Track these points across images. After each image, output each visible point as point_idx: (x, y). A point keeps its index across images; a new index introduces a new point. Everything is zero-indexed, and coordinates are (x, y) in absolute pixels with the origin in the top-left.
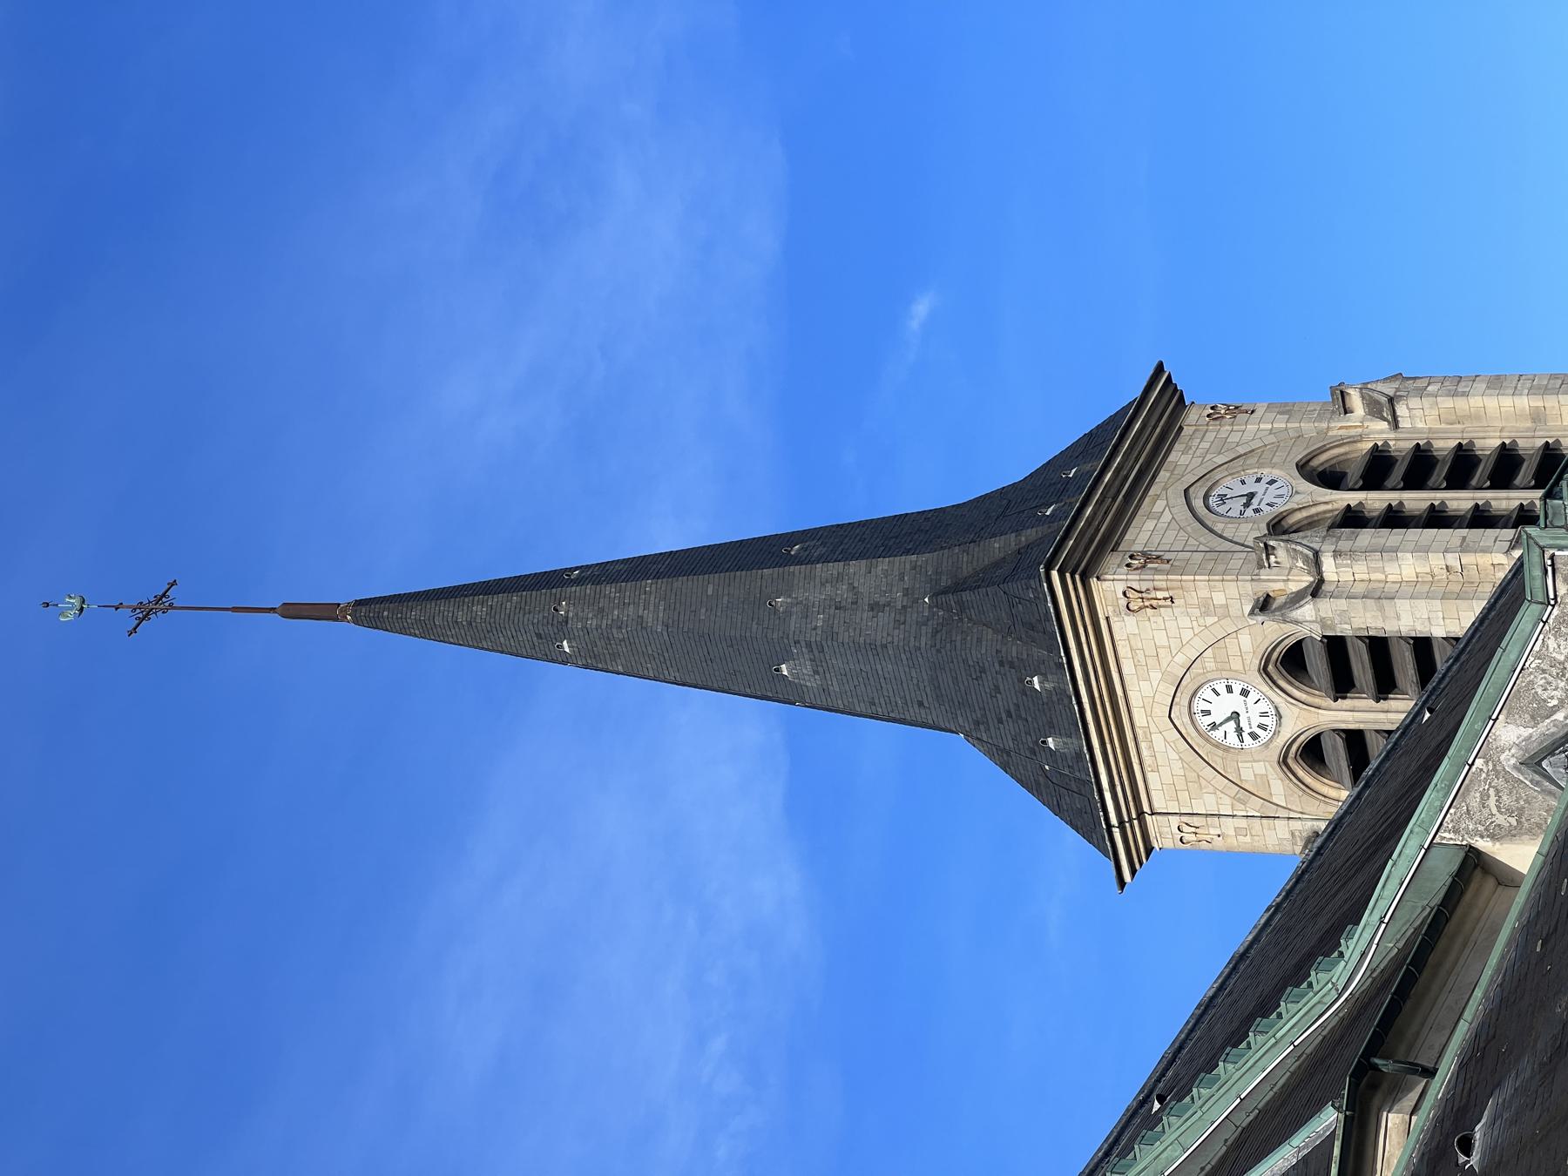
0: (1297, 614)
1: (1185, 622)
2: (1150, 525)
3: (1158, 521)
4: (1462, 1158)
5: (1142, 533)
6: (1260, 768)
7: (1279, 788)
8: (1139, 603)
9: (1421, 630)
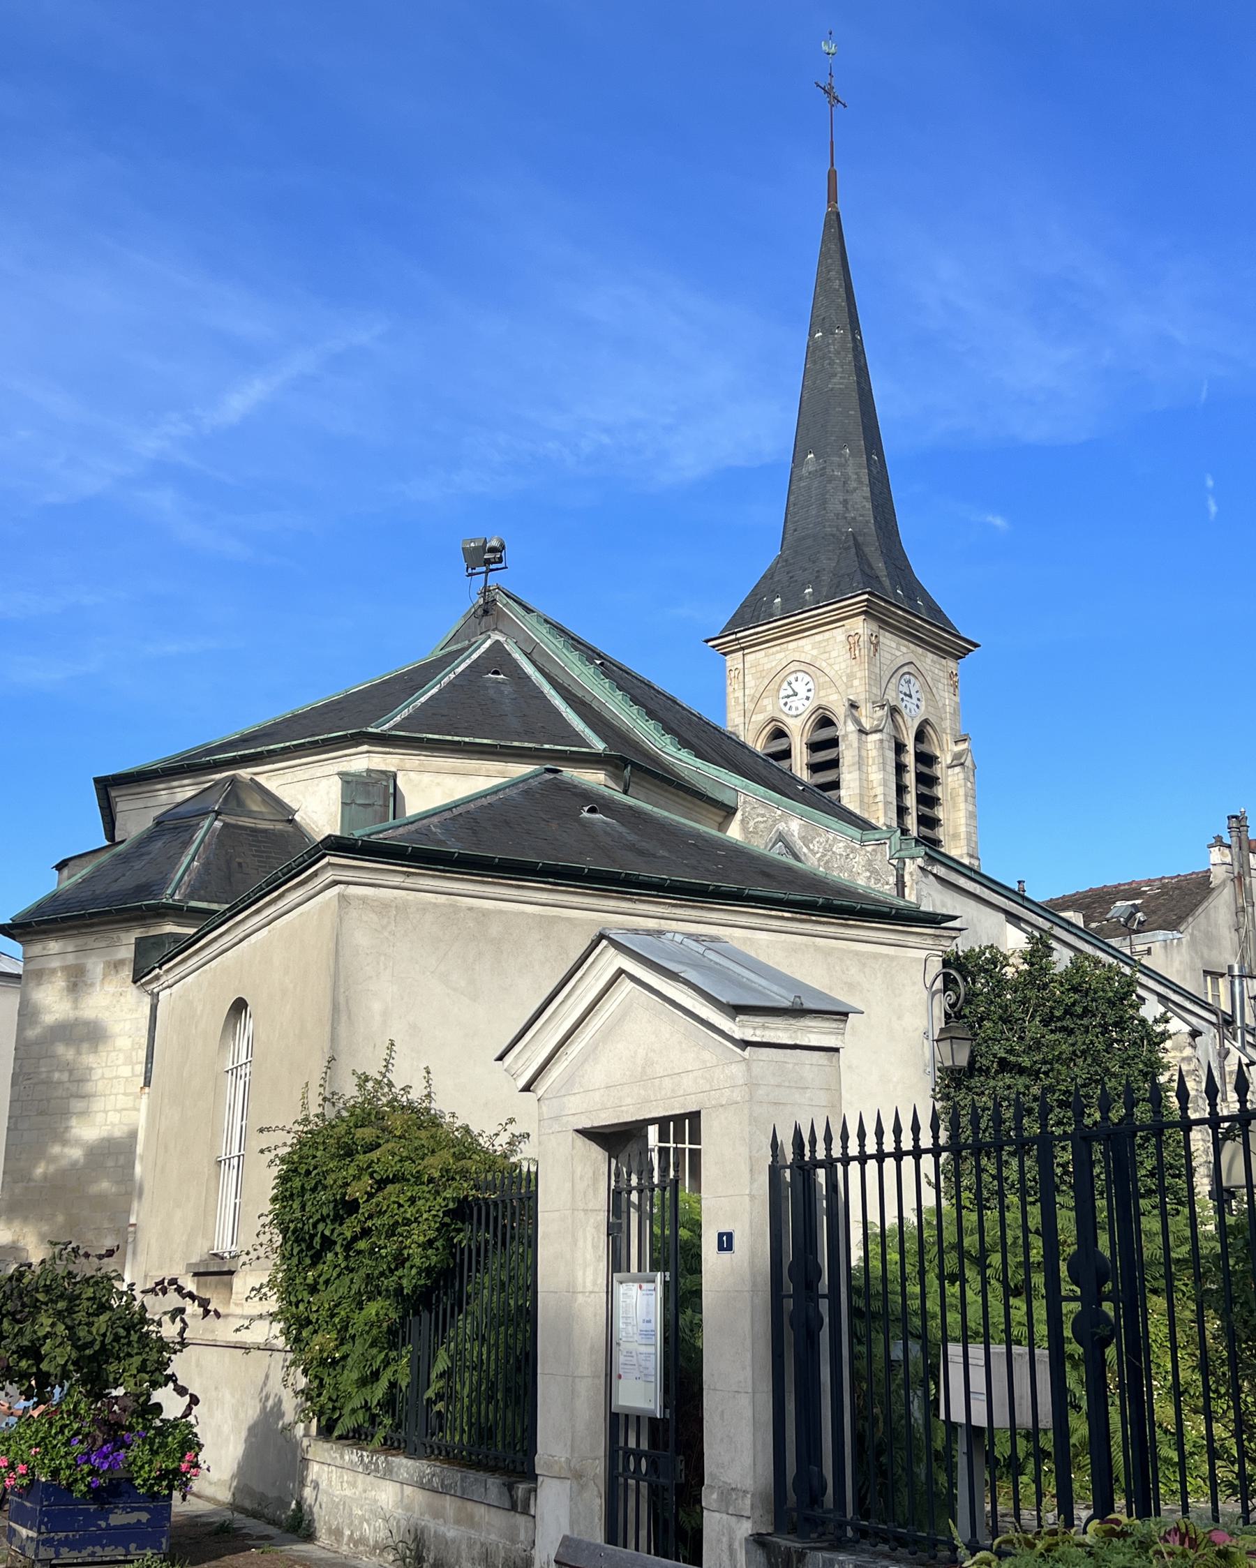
0: (849, 722)
1: (843, 666)
2: (894, 645)
3: (896, 649)
4: (586, 809)
5: (889, 641)
6: (769, 708)
7: (760, 718)
8: (852, 643)
9: (843, 784)
